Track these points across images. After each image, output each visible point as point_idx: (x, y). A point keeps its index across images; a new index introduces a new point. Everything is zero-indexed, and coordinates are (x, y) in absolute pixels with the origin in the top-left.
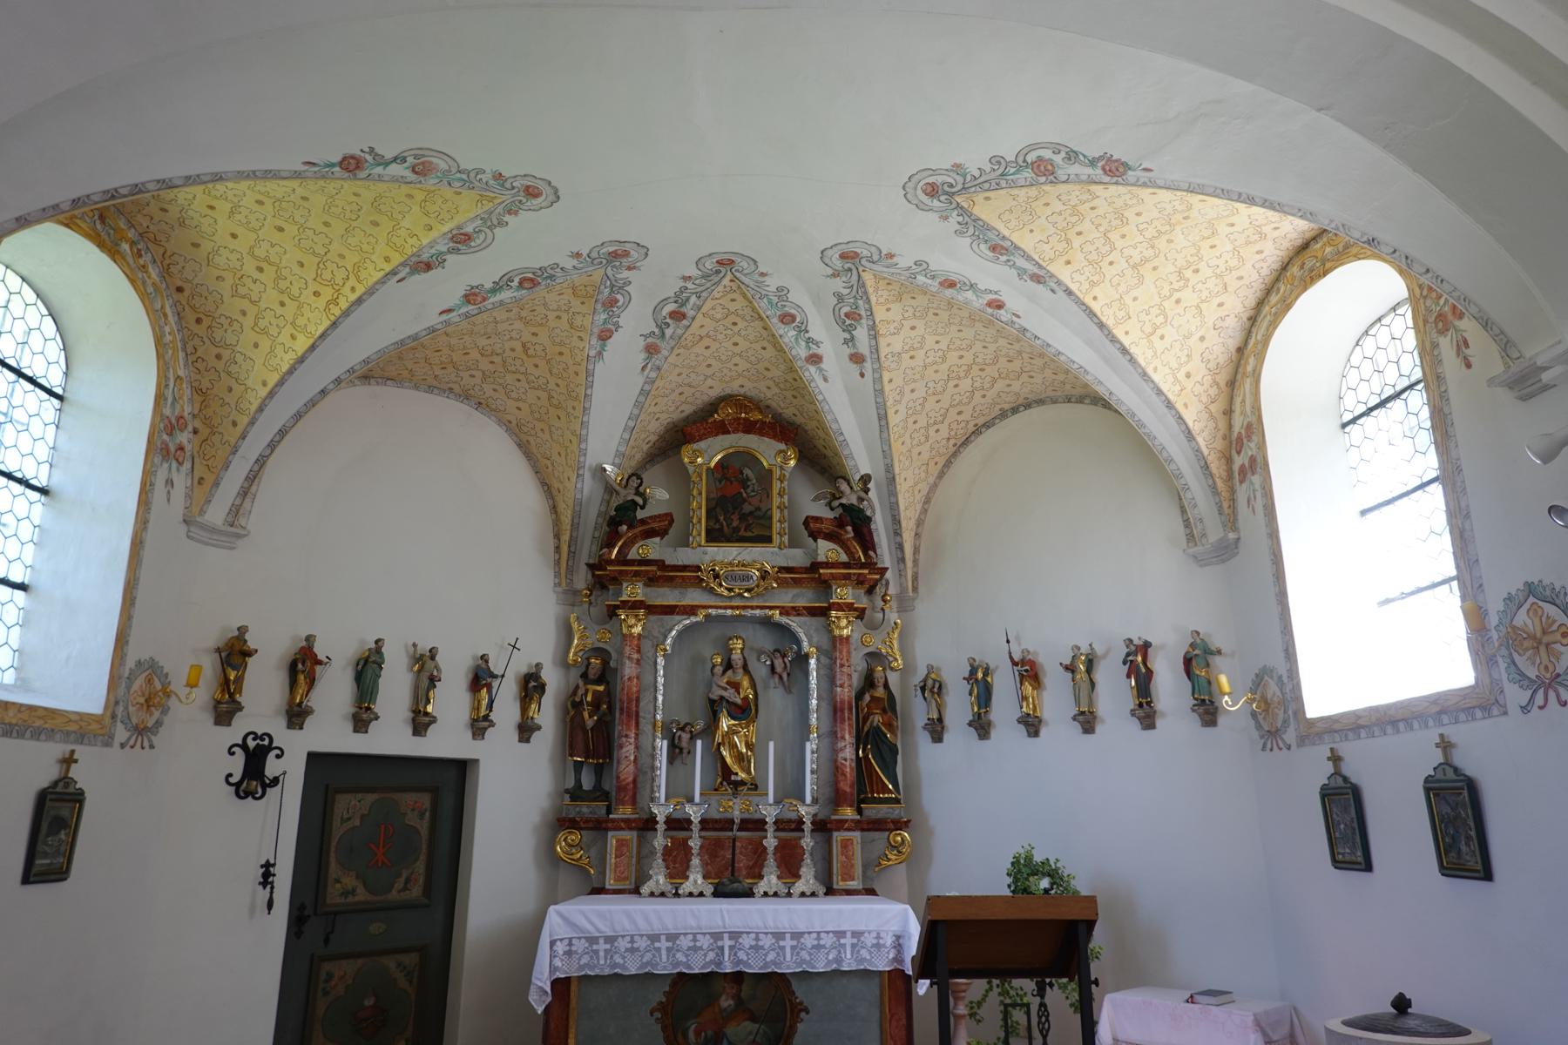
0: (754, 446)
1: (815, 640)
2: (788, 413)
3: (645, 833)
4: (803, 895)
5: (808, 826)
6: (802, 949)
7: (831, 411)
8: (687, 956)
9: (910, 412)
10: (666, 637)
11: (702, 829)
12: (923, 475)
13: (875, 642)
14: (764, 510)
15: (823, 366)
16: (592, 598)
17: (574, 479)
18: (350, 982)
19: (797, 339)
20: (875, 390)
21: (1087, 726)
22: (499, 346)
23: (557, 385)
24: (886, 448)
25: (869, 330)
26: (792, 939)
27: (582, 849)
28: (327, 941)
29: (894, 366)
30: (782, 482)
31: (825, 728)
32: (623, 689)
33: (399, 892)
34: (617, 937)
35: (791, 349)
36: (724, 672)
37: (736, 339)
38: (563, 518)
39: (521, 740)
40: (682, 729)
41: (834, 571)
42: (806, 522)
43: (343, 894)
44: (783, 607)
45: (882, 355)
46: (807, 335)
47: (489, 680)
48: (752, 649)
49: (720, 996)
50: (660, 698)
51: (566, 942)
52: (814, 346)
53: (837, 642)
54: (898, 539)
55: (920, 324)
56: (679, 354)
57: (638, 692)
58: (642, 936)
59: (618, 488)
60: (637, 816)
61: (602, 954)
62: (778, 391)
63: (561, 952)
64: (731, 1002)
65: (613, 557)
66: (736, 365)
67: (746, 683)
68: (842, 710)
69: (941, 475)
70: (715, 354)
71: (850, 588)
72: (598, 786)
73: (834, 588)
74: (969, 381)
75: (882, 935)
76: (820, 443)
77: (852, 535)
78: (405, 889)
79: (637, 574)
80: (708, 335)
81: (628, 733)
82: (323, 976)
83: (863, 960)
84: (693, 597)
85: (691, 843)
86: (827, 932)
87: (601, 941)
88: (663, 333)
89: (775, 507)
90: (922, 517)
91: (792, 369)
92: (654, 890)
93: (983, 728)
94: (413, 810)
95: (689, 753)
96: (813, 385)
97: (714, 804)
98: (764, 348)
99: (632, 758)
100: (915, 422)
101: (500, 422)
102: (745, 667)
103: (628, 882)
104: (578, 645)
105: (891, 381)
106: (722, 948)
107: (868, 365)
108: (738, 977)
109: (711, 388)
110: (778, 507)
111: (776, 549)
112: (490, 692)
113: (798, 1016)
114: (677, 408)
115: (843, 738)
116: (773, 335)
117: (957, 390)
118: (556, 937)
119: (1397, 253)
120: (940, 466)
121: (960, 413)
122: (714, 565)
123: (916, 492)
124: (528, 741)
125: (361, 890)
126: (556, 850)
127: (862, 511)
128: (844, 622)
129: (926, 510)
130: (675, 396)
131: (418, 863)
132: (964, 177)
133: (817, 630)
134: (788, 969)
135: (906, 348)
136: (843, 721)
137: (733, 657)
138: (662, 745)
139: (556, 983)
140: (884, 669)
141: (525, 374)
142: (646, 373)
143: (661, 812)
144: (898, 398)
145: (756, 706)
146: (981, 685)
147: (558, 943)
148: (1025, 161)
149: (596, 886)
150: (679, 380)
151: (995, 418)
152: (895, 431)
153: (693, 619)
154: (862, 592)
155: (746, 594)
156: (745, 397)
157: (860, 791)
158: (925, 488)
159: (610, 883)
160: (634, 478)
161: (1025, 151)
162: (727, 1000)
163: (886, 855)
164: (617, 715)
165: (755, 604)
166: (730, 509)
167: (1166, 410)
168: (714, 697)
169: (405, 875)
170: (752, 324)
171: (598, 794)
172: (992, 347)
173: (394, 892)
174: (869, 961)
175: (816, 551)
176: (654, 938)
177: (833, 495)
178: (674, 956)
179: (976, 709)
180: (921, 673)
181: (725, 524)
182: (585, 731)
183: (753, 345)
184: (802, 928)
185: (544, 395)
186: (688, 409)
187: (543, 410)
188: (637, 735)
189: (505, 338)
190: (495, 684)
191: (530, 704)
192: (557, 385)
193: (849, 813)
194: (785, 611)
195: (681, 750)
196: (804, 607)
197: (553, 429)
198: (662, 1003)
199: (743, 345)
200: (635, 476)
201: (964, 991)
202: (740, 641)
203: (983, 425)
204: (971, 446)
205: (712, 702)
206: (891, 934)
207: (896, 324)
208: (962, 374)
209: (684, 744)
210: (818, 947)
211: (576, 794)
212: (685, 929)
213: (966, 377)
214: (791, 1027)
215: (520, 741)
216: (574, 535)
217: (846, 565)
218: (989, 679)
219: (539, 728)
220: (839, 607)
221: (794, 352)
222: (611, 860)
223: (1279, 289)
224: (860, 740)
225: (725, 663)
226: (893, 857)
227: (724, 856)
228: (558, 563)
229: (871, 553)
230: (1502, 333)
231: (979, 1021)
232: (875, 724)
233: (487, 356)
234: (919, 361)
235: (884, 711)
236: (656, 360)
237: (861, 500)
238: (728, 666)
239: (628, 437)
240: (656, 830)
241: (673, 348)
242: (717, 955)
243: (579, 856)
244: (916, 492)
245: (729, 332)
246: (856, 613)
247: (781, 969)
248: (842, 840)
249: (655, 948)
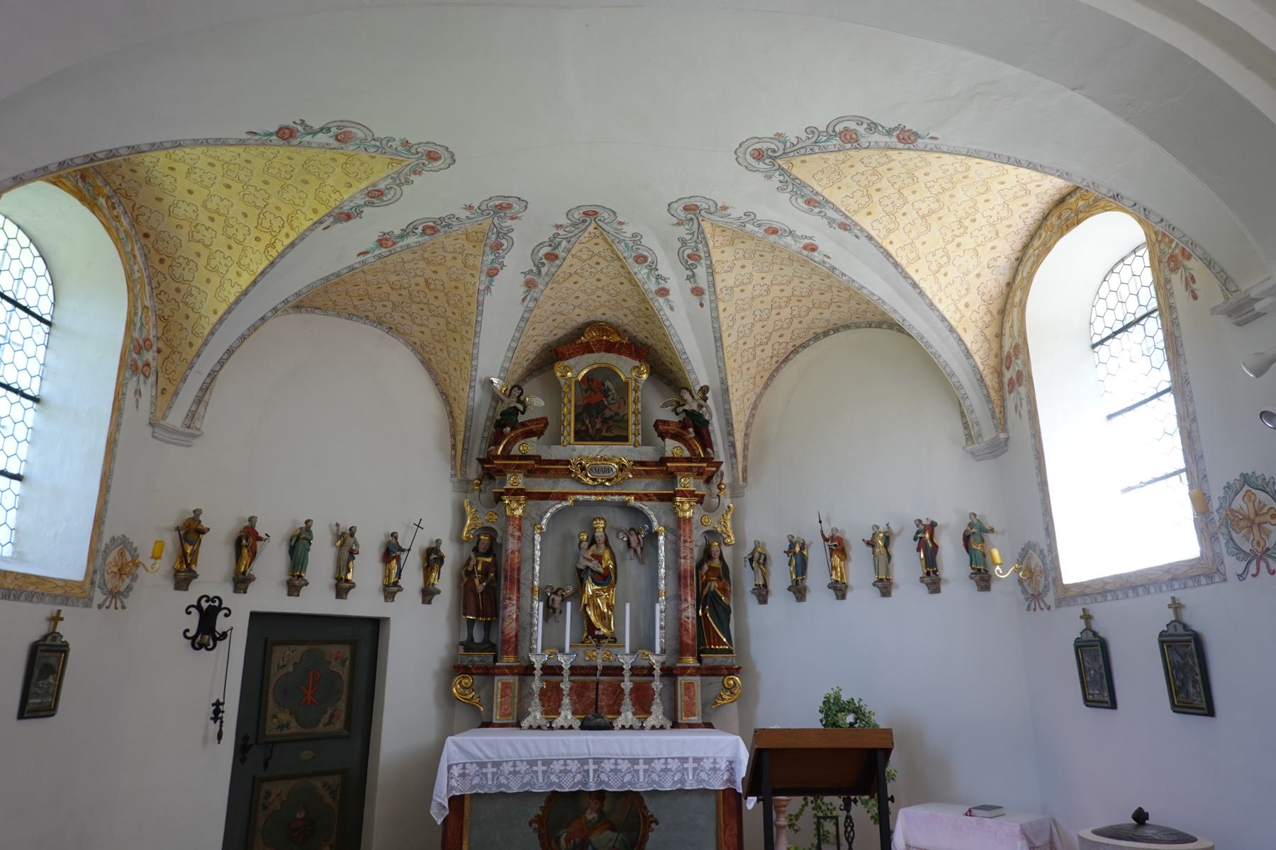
0: (614, 363)
1: (663, 520)
2: (641, 336)
3: (525, 678)
4: (653, 728)
5: (657, 672)
6: (652, 772)
7: (676, 334)
8: (559, 777)
9: (741, 335)
10: (542, 519)
11: (571, 675)
12: (751, 386)
13: (712, 523)
14: (621, 415)
15: (669, 297)
16: (482, 486)
17: (467, 390)
18: (285, 798)
19: (648, 276)
20: (712, 317)
22: (406, 281)
23: (454, 313)
24: (721, 365)
25: (707, 268)
26: (645, 763)
27: (473, 690)
28: (266, 765)
29: (727, 297)
30: (636, 392)
31: (672, 592)
32: (507, 561)
33: (325, 725)
34: (502, 762)
35: (644, 284)
36: (589, 547)
37: (599, 275)
38: (458, 421)
39: (424, 602)
40: (555, 593)
41: (678, 464)
42: (656, 425)
43: (279, 727)
44: (637, 494)
45: (718, 289)
46: (657, 273)
47: (398, 553)
48: (612, 528)
49: (586, 810)
50: (537, 568)
51: (461, 766)
52: (662, 282)
53: (681, 522)
54: (731, 438)
55: (748, 264)
56: (552, 288)
57: (519, 562)
58: (522, 761)
59: (503, 397)
60: (518, 664)
61: (490, 776)
62: (633, 318)
63: (456, 775)
64: (595, 815)
65: (499, 453)
66: (599, 297)
67: (607, 556)
68: (685, 578)
69: (766, 386)
70: (582, 288)
71: (692, 478)
72: (486, 639)
73: (679, 478)
74: (788, 310)
75: (717, 761)
76: (667, 361)
77: (693, 435)
78: (330, 723)
79: (518, 467)
80: (576, 273)
81: (511, 596)
82: (263, 794)
83: (702, 781)
84: (564, 485)
85: (562, 686)
86: (673, 758)
87: (489, 765)
88: (540, 271)
89: (630, 413)
90: (751, 421)
91: (644, 300)
92: (532, 724)
93: (800, 592)
94: (336, 659)
95: (561, 612)
96: (661, 313)
97: (581, 654)
98: (622, 283)
99: (514, 616)
100: (745, 343)
101: (407, 343)
102: (606, 543)
103: (511, 718)
104: (470, 525)
105: (725, 310)
106: (587, 771)
107: (706, 297)
108: (601, 795)
109: (578, 315)
110: (633, 413)
111: (632, 447)
112: (398, 563)
113: (649, 827)
114: (551, 332)
115: (686, 600)
116: (629, 273)
117: (779, 317)
118: (452, 763)
119: (1137, 206)
120: (765, 379)
121: (781, 336)
122: (581, 459)
123: (746, 400)
124: (429, 602)
125: (293, 724)
126: (452, 691)
127: (701, 416)
128: (687, 506)
129: (754, 415)
130: (549, 322)
131: (340, 702)
132: (785, 144)
133: (665, 512)
134: (641, 788)
135: (738, 283)
136: (686, 586)
137: (597, 534)
138: (539, 606)
139: (452, 800)
140: (719, 545)
141: (427, 304)
142: (525, 303)
143: (538, 661)
144: (731, 324)
145: (616, 574)
146: (799, 557)
147: (454, 767)
148: (834, 131)
149: (485, 720)
150: (553, 309)
151: (810, 340)
152: (728, 351)
153: (564, 504)
154: (701, 481)
155: (607, 484)
156: (607, 323)
157: (700, 644)
158: (752, 397)
159: (496, 718)
160: (516, 389)
162: (591, 813)
163: (721, 696)
164: (502, 581)
165: (614, 491)
166: (594, 414)
167: (949, 333)
168: (581, 567)
169: (329, 712)
170: (612, 264)
171: (487, 646)
172: (807, 283)
173: (321, 726)
174: (707, 782)
175: (664, 448)
176: (532, 763)
177: (678, 403)
178: (548, 777)
179: (794, 577)
180: (750, 547)
181: (590, 426)
182: (476, 594)
183: (612, 281)
184: (653, 755)
185: (442, 321)
186: (560, 333)
187: (442, 334)
188: (518, 597)
189: (411, 275)
190: (403, 556)
191: (432, 573)
192: (454, 313)
193: (691, 661)
194: (639, 497)
195: (554, 610)
196: (654, 494)
197: (450, 349)
198: (539, 816)
199: (605, 280)
200: (517, 387)
201: (785, 806)
202: (602, 522)
203: (800, 346)
204: (790, 363)
205: (579, 571)
206: (725, 760)
207: (729, 264)
208: (783, 305)
209: (557, 605)
210: (666, 770)
211: (469, 646)
212: (558, 755)
213: (786, 306)
214: (643, 835)
215: (423, 603)
216: (467, 435)
217: (688, 460)
218: (805, 553)
219: (438, 592)
220: (683, 494)
221: (646, 287)
222: (498, 699)
223: (1040, 235)
224: (700, 602)
225: (590, 540)
226: (727, 697)
227: (589, 697)
228: (454, 458)
229: (709, 450)
230: (1222, 271)
231: (797, 830)
232: (712, 589)
233: (396, 289)
234: (748, 294)
235: (720, 578)
236: (534, 293)
237: (701, 406)
238: (593, 541)
239: (511, 355)
240: (534, 675)
241: (547, 283)
242: (584, 777)
243: (471, 696)
244: (746, 400)
245: (593, 270)
246: (697, 499)
247: (635, 788)
248: (685, 683)
249: (533, 771)
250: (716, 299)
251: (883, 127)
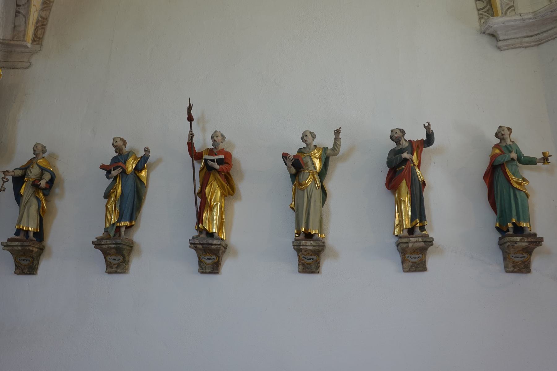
21: (414, 259)
146: (130, 181)
179: (114, 220)
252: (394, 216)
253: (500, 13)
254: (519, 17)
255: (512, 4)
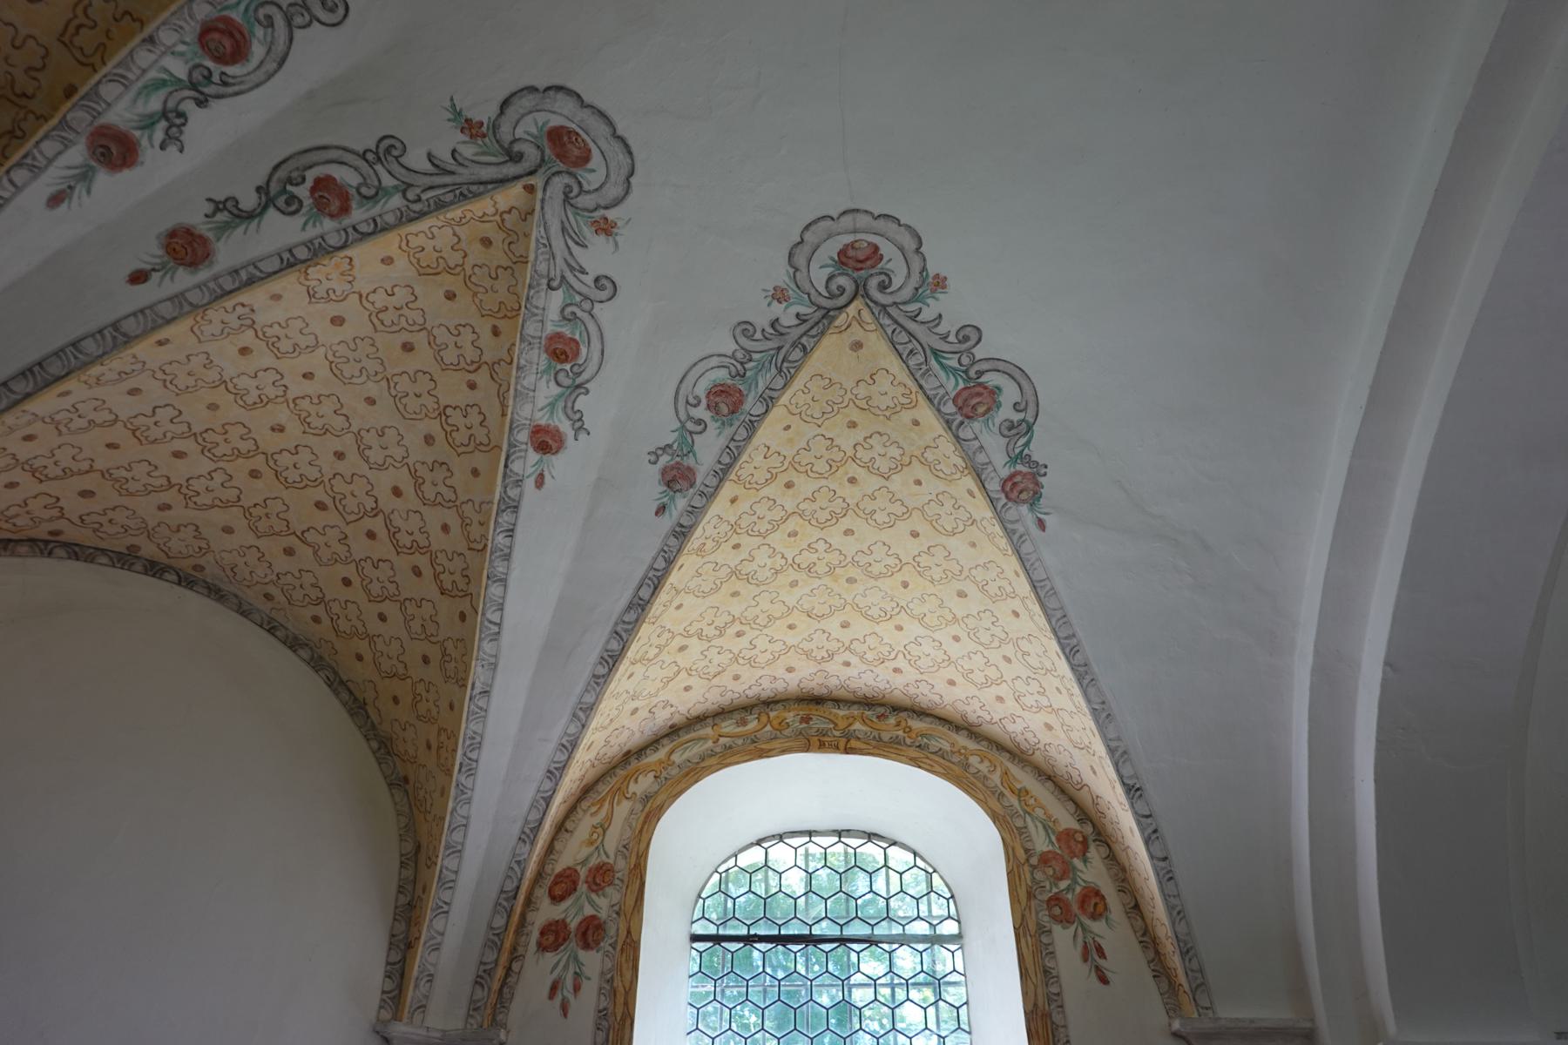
19: (159, 84)
25: (308, 244)
35: (121, 79)
45: (244, 297)
46: (189, 107)
52: (159, 135)
107: (184, 279)
119: (1149, 820)
132: (915, 298)
148: (980, 373)
151: (104, 551)
161: (1001, 366)
167: (540, 773)
203: (65, 545)
221: (109, 91)
223: (744, 723)
230: (1201, 971)
250: (195, 307)
251: (1027, 444)
252: (972, 1024)
253: (405, 1020)
254: (423, 1032)
255: (424, 1003)
